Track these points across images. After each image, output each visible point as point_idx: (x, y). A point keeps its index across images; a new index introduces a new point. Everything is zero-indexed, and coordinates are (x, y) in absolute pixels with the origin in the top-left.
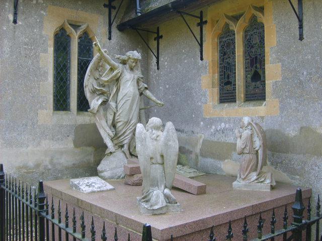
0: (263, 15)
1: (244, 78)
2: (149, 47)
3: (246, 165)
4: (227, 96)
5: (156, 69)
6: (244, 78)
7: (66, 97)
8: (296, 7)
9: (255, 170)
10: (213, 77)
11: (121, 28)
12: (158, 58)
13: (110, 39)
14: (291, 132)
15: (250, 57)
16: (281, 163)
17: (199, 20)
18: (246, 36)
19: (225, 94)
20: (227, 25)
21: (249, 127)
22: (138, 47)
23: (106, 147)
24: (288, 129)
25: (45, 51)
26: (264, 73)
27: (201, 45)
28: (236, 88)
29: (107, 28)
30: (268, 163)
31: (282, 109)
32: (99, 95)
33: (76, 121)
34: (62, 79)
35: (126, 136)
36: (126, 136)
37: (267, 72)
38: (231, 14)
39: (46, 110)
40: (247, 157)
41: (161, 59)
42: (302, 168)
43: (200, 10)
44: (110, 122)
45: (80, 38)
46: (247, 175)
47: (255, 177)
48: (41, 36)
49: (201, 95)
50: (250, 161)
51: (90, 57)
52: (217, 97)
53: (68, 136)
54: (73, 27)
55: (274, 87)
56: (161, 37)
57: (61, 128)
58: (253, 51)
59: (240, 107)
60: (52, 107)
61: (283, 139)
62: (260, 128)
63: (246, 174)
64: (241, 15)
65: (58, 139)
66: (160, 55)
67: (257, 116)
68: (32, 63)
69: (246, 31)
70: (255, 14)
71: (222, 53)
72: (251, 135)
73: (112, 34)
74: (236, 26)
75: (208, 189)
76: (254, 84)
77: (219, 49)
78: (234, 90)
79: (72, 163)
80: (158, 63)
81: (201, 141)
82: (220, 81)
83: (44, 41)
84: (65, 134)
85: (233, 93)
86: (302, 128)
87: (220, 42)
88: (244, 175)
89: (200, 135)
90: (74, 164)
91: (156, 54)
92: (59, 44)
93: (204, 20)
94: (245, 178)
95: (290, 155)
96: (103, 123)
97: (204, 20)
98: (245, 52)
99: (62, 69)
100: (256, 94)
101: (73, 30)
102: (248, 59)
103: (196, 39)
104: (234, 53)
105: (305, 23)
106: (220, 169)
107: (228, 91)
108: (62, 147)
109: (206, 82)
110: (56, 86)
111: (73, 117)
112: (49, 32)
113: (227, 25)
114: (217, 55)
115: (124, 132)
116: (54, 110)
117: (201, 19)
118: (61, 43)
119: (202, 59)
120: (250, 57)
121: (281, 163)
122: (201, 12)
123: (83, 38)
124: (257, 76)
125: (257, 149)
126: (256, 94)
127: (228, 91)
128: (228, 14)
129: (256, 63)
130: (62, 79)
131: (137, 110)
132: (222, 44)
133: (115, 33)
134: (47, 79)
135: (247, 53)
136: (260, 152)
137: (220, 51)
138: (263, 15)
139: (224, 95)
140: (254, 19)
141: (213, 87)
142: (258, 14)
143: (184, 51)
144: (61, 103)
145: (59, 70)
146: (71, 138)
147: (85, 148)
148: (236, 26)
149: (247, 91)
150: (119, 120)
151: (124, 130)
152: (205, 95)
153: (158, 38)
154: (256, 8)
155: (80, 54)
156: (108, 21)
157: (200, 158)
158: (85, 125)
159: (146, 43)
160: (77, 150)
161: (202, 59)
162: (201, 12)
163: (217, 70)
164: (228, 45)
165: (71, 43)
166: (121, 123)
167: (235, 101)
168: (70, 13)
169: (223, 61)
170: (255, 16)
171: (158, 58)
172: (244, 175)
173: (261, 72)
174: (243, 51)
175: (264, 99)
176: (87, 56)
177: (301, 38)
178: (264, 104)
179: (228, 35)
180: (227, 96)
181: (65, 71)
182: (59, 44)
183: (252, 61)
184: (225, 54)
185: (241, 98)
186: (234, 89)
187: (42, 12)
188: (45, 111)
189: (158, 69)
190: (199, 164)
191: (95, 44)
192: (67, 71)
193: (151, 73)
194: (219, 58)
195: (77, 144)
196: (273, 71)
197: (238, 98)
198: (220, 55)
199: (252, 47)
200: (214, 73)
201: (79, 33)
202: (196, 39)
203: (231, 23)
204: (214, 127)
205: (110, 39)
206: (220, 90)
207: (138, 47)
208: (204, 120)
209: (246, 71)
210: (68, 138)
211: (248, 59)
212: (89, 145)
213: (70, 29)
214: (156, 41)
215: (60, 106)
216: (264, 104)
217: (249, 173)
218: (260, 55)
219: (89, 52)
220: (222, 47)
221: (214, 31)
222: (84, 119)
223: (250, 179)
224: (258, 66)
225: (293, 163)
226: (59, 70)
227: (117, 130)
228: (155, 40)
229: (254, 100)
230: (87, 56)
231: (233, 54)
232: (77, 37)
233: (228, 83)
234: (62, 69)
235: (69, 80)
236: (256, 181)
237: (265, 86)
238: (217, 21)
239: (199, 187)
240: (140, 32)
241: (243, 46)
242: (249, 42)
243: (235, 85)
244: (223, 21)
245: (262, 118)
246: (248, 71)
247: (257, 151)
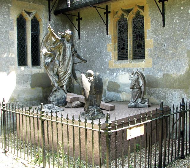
0: (144, 11)
1: (131, 45)
2: (73, 24)
3: (135, 95)
4: (122, 56)
5: (78, 38)
6: (131, 45)
7: (25, 57)
8: (162, 11)
9: (140, 97)
10: (114, 45)
11: (56, 13)
12: (79, 32)
13: (50, 20)
14: (159, 76)
15: (136, 34)
16: (154, 93)
17: (106, 10)
18: (134, 22)
19: (122, 54)
20: (123, 15)
21: (137, 74)
22: (66, 25)
23: (53, 86)
24: (157, 75)
25: (12, 29)
26: (144, 43)
27: (107, 26)
28: (128, 51)
29: (48, 13)
30: (146, 93)
31: (154, 64)
32: (48, 56)
33: (31, 72)
34: (22, 46)
35: (65, 80)
36: (65, 80)
37: (145, 44)
38: (125, 9)
39: (14, 65)
40: (136, 90)
41: (81, 33)
42: (165, 95)
43: (106, 4)
44: (55, 72)
45: (31, 20)
46: (136, 100)
47: (140, 101)
48: (10, 20)
49: (107, 55)
50: (137, 92)
51: (38, 32)
52: (116, 57)
53: (27, 81)
54: (27, 13)
55: (150, 52)
56: (81, 19)
57: (23, 76)
58: (138, 31)
59: (131, 62)
60: (17, 64)
61: (154, 80)
62: (142, 74)
63: (135, 99)
64: (131, 10)
65: (22, 83)
66: (80, 30)
67: (140, 67)
68: (5, 37)
69: (133, 19)
70: (139, 10)
71: (119, 31)
72: (138, 78)
73: (51, 17)
74: (128, 16)
75: (115, 108)
76: (138, 49)
77: (117, 29)
78: (126, 52)
79: (30, 97)
80: (79, 35)
81: (108, 82)
82: (118, 47)
83: (12, 23)
84: (25, 80)
85: (127, 57)
86: (164, 74)
87: (118, 24)
88: (134, 100)
89: (107, 79)
90: (31, 98)
91: (78, 29)
92: (19, 24)
93: (109, 11)
94: (135, 102)
95: (158, 89)
96: (52, 73)
97: (109, 11)
98: (133, 31)
99: (22, 40)
100: (139, 55)
101: (28, 16)
102: (135, 35)
103: (104, 23)
104: (127, 31)
105: (166, 18)
106: (119, 98)
107: (123, 53)
108: (24, 88)
109: (110, 47)
110: (19, 51)
111: (29, 70)
112: (14, 17)
113: (123, 15)
114: (116, 32)
115: (64, 78)
116: (18, 66)
117: (107, 10)
118: (21, 23)
119: (107, 34)
120: (136, 34)
121: (154, 93)
122: (107, 6)
123: (34, 20)
124: (139, 38)
125: (141, 86)
126: (139, 55)
127: (123, 53)
128: (123, 8)
129: (139, 38)
130: (22, 46)
131: (72, 65)
132: (119, 25)
133: (53, 16)
134: (14, 47)
135: (134, 31)
136: (142, 88)
137: (118, 29)
138: (144, 11)
139: (121, 55)
140: (138, 14)
141: (114, 51)
142: (141, 10)
143: (96, 28)
144: (22, 61)
145: (20, 40)
146: (29, 82)
147: (37, 88)
148: (128, 16)
149: (134, 54)
150: (60, 71)
151: (64, 77)
152: (109, 55)
153: (79, 19)
154: (139, 7)
155: (32, 30)
156: (48, 9)
157: (107, 92)
158: (36, 74)
159: (71, 21)
160: (33, 90)
161: (107, 34)
162: (107, 6)
163: (116, 40)
164: (123, 26)
165: (27, 24)
166: (62, 73)
167: (128, 59)
168: (29, 6)
169: (120, 36)
170: (138, 11)
171: (79, 32)
172: (134, 100)
173: (142, 43)
174: (132, 31)
175: (144, 58)
176: (36, 31)
177: (164, 26)
178: (144, 61)
179: (123, 21)
180: (122, 56)
181: (23, 41)
182: (19, 24)
183: (137, 36)
184: (121, 32)
185: (131, 57)
186: (127, 52)
187: (9, 5)
188: (13, 66)
189: (79, 38)
190: (106, 95)
191: (49, 28)
192: (24, 41)
193: (75, 41)
194: (117, 33)
195: (32, 87)
196: (149, 42)
197: (129, 57)
198: (118, 32)
199: (137, 28)
200: (115, 42)
201: (31, 17)
202: (104, 23)
203: (125, 14)
204: (115, 74)
205: (50, 20)
206: (119, 52)
207: (66, 25)
208: (109, 70)
209: (134, 42)
210: (27, 82)
211: (135, 35)
212: (39, 86)
213: (25, 15)
214: (78, 21)
215: (21, 63)
216: (144, 61)
217: (137, 99)
218: (142, 33)
219: (37, 29)
220: (120, 27)
221: (115, 18)
222: (36, 70)
223: (137, 102)
224: (141, 39)
225: (159, 93)
226: (20, 40)
227: (59, 77)
228: (77, 20)
229: (138, 59)
230: (36, 31)
231: (126, 31)
232: (30, 20)
233: (123, 48)
234: (22, 40)
235: (26, 46)
236: (141, 103)
237: (144, 51)
238: (117, 12)
239: (111, 106)
240: (68, 15)
241: (132, 27)
242: (135, 25)
243: (128, 49)
244: (120, 13)
245: (143, 69)
246: (135, 42)
247: (141, 87)
